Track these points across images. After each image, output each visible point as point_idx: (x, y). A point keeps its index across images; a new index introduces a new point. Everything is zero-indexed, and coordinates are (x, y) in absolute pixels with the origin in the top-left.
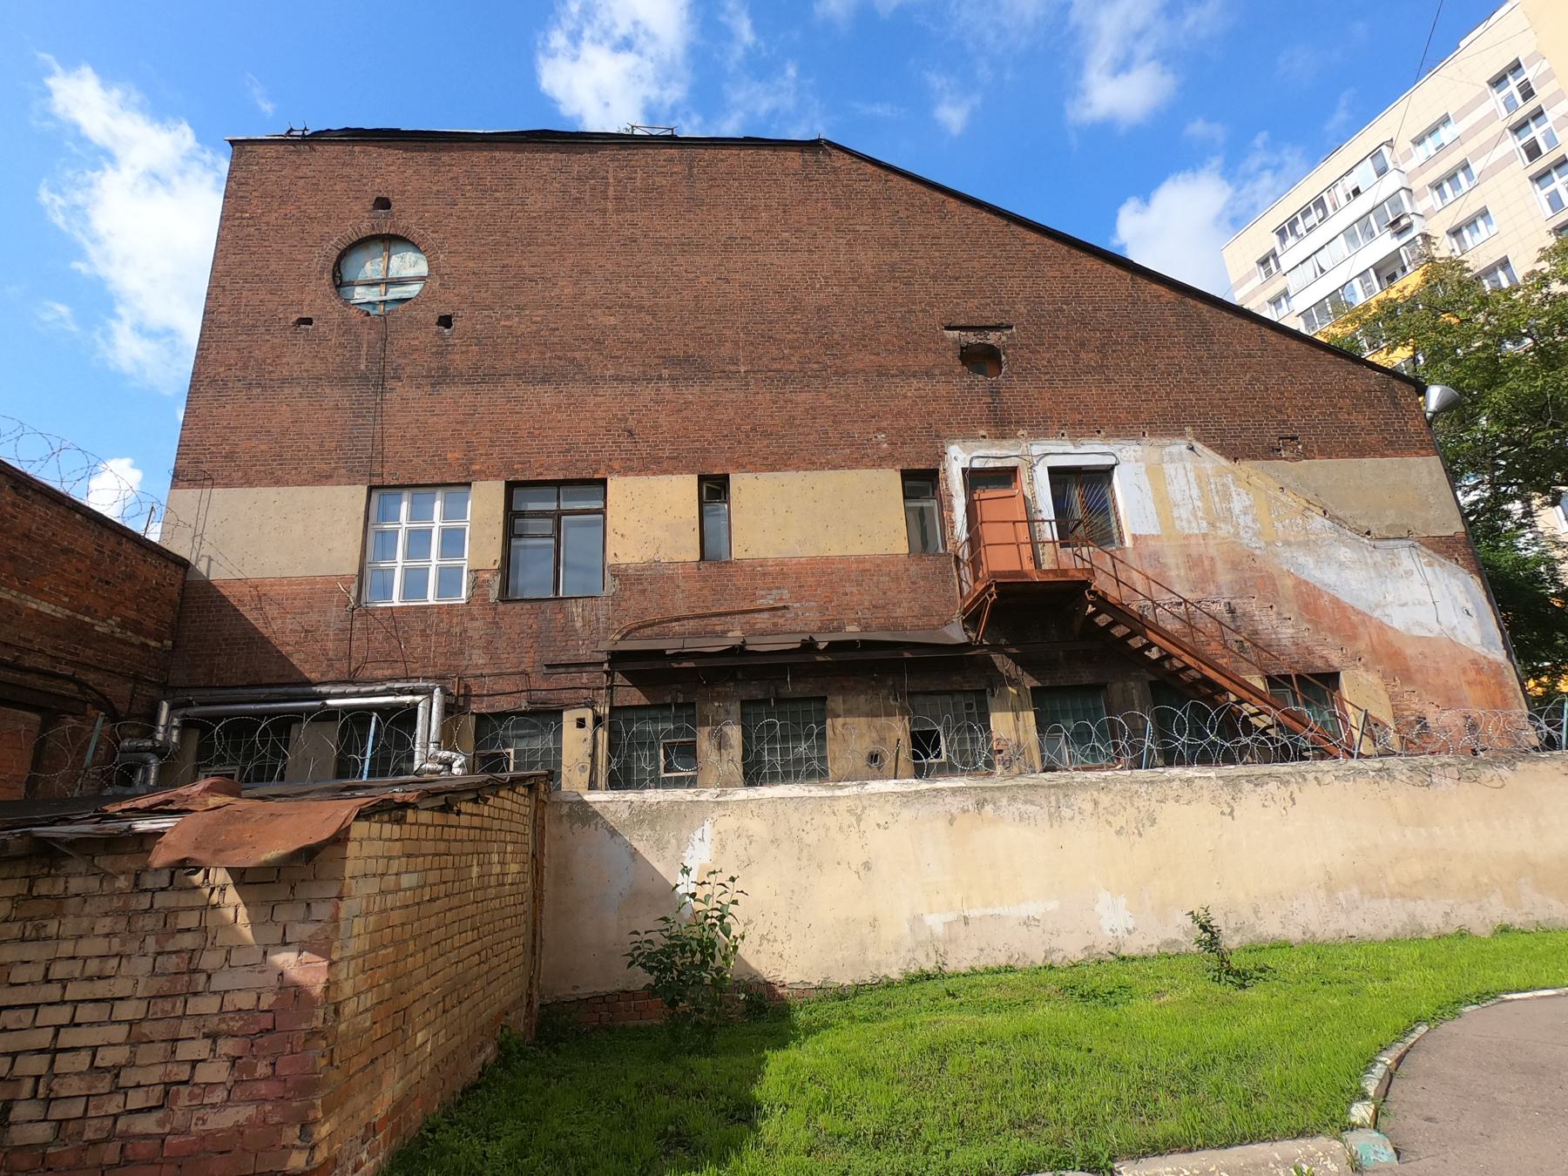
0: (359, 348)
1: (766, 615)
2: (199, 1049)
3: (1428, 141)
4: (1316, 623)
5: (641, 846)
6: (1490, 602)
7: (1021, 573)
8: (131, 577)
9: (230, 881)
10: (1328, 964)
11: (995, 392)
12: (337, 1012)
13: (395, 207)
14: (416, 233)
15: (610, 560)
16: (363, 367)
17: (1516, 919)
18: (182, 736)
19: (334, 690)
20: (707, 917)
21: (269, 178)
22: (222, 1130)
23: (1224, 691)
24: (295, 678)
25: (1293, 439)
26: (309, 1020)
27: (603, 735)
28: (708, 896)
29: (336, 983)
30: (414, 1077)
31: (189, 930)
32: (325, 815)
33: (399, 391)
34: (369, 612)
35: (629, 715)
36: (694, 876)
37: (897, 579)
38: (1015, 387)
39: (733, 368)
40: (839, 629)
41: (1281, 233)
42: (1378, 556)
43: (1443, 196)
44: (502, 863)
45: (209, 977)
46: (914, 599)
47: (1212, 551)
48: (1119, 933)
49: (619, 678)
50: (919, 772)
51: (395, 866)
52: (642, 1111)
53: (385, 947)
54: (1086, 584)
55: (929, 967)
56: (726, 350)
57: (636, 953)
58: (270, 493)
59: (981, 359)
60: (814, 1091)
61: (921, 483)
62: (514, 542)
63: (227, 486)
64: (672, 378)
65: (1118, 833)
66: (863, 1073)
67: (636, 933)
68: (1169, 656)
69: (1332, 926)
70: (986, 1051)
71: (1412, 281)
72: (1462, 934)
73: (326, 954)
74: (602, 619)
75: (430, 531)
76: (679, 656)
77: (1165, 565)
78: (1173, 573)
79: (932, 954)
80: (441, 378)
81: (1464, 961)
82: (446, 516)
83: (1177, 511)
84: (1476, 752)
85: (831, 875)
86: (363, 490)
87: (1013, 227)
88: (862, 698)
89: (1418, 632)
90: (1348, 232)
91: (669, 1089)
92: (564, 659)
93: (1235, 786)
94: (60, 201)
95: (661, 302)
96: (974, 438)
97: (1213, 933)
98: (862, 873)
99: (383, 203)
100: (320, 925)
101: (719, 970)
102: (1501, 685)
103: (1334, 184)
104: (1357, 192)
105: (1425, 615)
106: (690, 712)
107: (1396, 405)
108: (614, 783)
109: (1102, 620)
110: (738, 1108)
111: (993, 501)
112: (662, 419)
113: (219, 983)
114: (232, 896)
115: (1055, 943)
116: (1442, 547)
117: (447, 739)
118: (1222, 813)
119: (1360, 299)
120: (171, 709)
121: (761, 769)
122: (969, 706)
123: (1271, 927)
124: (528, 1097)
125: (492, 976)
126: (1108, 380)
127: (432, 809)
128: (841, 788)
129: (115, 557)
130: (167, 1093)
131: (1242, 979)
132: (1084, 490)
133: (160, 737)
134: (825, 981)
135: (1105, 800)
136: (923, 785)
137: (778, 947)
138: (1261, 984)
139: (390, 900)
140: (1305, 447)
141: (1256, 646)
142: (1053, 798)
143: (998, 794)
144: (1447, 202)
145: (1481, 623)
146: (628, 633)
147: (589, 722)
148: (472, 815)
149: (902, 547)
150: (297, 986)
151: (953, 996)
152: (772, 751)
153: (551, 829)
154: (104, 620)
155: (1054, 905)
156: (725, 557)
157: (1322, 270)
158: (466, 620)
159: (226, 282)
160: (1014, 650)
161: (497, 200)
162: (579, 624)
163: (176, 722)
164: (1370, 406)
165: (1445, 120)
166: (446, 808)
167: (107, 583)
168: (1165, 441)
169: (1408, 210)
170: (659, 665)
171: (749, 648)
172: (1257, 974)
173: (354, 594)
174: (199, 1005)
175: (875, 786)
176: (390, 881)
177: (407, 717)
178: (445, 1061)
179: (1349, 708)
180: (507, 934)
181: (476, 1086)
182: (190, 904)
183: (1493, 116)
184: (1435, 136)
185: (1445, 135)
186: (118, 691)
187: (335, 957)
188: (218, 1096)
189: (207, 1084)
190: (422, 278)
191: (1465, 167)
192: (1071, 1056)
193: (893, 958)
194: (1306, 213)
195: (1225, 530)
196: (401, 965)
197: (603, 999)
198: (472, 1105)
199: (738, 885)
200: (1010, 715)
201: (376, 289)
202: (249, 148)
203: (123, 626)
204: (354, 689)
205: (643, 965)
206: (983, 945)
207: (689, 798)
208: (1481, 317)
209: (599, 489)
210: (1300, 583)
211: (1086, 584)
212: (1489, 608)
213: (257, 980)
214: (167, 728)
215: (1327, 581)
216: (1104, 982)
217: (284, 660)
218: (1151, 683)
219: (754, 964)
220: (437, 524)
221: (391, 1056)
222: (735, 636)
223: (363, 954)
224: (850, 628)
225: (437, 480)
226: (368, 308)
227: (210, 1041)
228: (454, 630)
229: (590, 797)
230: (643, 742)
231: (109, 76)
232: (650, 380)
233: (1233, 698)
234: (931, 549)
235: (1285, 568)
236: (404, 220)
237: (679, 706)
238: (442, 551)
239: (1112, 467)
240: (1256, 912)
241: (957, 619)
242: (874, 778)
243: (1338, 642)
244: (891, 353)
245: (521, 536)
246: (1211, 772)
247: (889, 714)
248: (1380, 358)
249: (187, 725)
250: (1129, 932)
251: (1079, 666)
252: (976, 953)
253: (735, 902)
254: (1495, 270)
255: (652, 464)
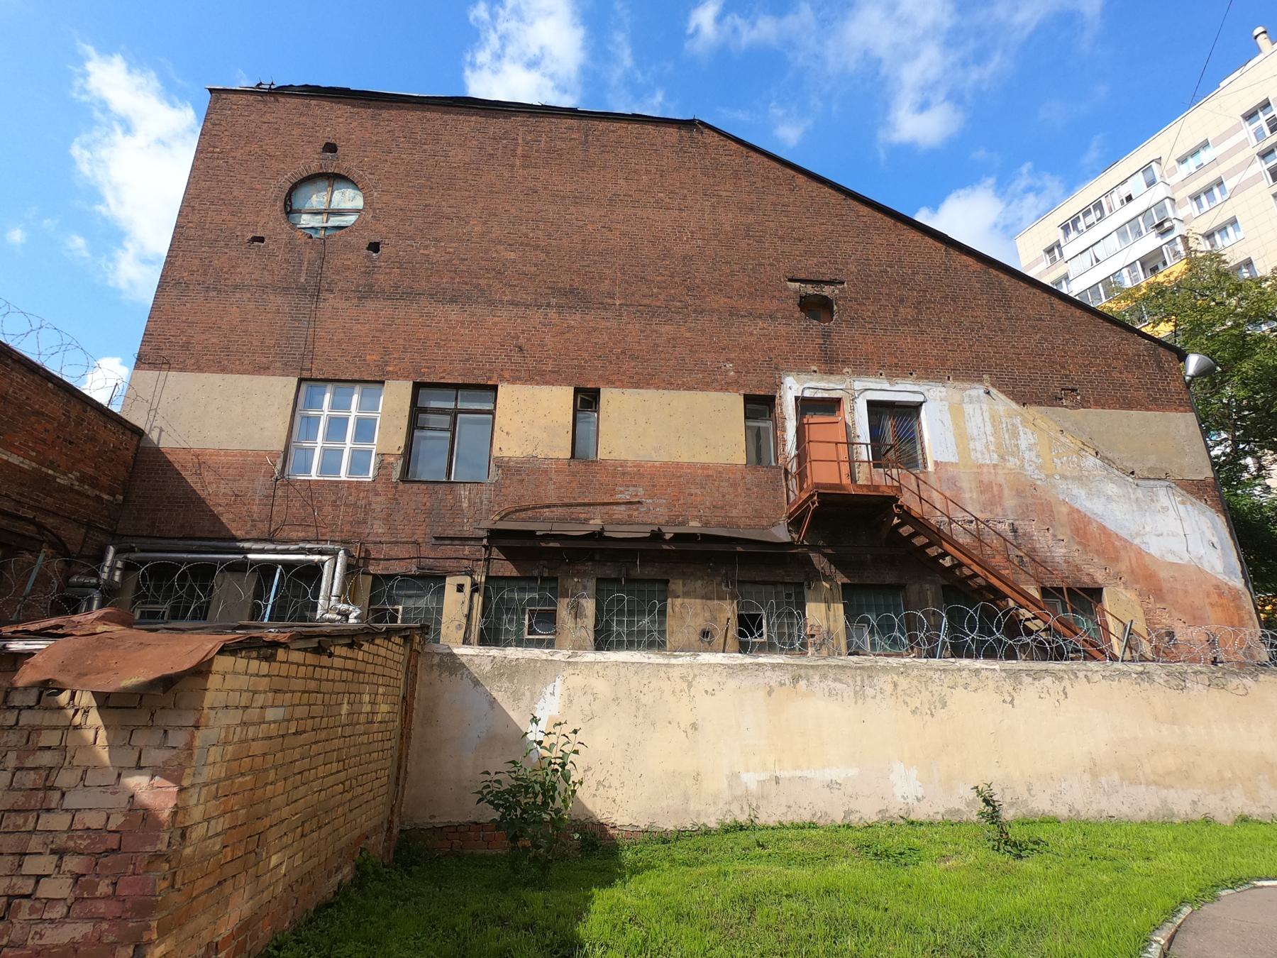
0: (301, 264)
1: (623, 508)
2: (44, 864)
3: (1190, 160)
4: (1085, 546)
5: (500, 697)
6: (1233, 538)
7: (839, 486)
8: (92, 439)
9: (94, 704)
10: (1095, 841)
11: (826, 335)
12: (183, 836)
13: (340, 151)
14: (355, 174)
15: (496, 453)
16: (302, 280)
17: (1255, 811)
18: (123, 577)
19: (255, 546)
20: (550, 763)
21: (232, 119)
22: (57, 946)
23: (1005, 597)
24: (223, 534)
25: (1073, 390)
26: (153, 843)
27: (478, 599)
28: (552, 745)
29: (184, 808)
30: (266, 896)
31: (49, 748)
32: (190, 648)
33: (331, 302)
34: (290, 483)
35: (502, 584)
36: (543, 725)
37: (734, 485)
38: (843, 332)
39: (609, 301)
40: (683, 524)
41: (1065, 228)
42: (1139, 493)
43: (1200, 206)
44: (373, 703)
45: (63, 795)
46: (748, 503)
47: (1001, 480)
48: (909, 801)
49: (495, 553)
50: (744, 648)
51: (260, 699)
52: (474, 941)
53: (242, 774)
54: (894, 499)
55: (743, 819)
56: (605, 286)
57: (485, 792)
58: (216, 378)
59: (817, 307)
60: (634, 932)
61: (760, 406)
62: (417, 433)
63: (181, 370)
64: (559, 306)
65: (914, 712)
66: (679, 918)
67: (488, 773)
68: (960, 565)
69: (1094, 806)
70: (794, 905)
71: (1175, 269)
72: (1208, 821)
73: (177, 780)
74: (485, 502)
75: (347, 419)
76: (548, 537)
77: (960, 488)
78: (967, 495)
79: (746, 808)
80: (367, 293)
81: (1215, 846)
82: (361, 407)
83: (974, 445)
84: (1218, 663)
85: (658, 732)
86: (294, 381)
87: (850, 201)
88: (699, 583)
89: (1171, 558)
90: (1121, 231)
91: (502, 921)
92: (451, 533)
93: (1016, 678)
94: (87, 154)
95: (554, 243)
96: (807, 372)
97: (994, 807)
98: (690, 732)
99: (331, 148)
100: (174, 752)
101: (558, 811)
102: (1238, 608)
103: (1111, 191)
104: (1129, 198)
105: (1177, 545)
106: (553, 585)
107: (1161, 368)
108: (483, 641)
109: (906, 530)
110: (563, 945)
111: (818, 424)
112: (548, 340)
113: (71, 801)
114: (94, 718)
115: (854, 805)
116: (1194, 489)
117: (349, 593)
118: (1004, 701)
119: (1128, 284)
120: (116, 553)
121: (609, 636)
122: (789, 596)
123: (1041, 804)
124: (373, 919)
125: (355, 803)
126: (922, 332)
127: (305, 650)
128: (676, 657)
129: (80, 421)
130: (9, 905)
131: (1018, 849)
132: (894, 422)
133: (105, 576)
134: (650, 826)
135: (903, 683)
136: (747, 659)
137: (612, 793)
138: (1036, 855)
139: (251, 732)
140: (1083, 398)
141: (1035, 560)
142: (859, 678)
143: (811, 672)
144: (1203, 210)
145: (1224, 555)
146: (506, 515)
147: (467, 589)
148: (345, 658)
149: (741, 459)
150: (146, 809)
151: (763, 846)
152: (620, 623)
153: (422, 676)
154: (65, 474)
155: (854, 772)
156: (592, 457)
157: (1097, 260)
158: (370, 495)
159: (196, 203)
160: (830, 551)
161: (425, 151)
162: (465, 505)
163: (119, 564)
164: (1139, 367)
165: (1205, 144)
166: (319, 650)
167: (71, 443)
168: (966, 385)
169: (1171, 215)
170: (529, 543)
171: (606, 534)
172: (1031, 846)
173: (279, 467)
174: (47, 822)
175: (706, 658)
176: (254, 714)
177: (314, 572)
178: (301, 881)
179: (1109, 619)
180: (373, 766)
181: (329, 905)
182: (54, 723)
183: (1244, 144)
184: (1196, 157)
185: (1205, 156)
186: (72, 535)
187: (185, 783)
188: (58, 912)
189: (48, 899)
190: (358, 211)
191: (1220, 183)
192: (868, 914)
193: (711, 809)
194: (1087, 213)
195: (1012, 462)
196: (259, 792)
197: (456, 828)
198: (321, 924)
199: (580, 737)
200: (823, 606)
201: (319, 217)
202: (224, 96)
203: (82, 480)
204: (271, 546)
205: (491, 803)
206: (792, 803)
207: (544, 657)
208: (1233, 301)
209: (490, 394)
210: (1074, 511)
211: (894, 499)
212: (1231, 542)
213: (109, 801)
214: (113, 568)
215: (1096, 511)
216: (895, 844)
217: (215, 518)
218: (943, 587)
219: (590, 806)
220: (353, 413)
221: (242, 878)
222: (595, 524)
223: (219, 781)
224: (692, 524)
225: (356, 377)
226: (311, 232)
227: (56, 857)
228: (359, 503)
229: (460, 650)
230: (508, 606)
231: (136, 62)
232: (539, 307)
233: (1011, 604)
234: (765, 462)
235: (1061, 497)
236: (346, 162)
237: (544, 579)
238: (353, 438)
239: (921, 404)
240: (1029, 790)
241: (783, 521)
242: (706, 651)
243: (1103, 562)
244: (742, 297)
245: (423, 428)
246: (996, 665)
247: (721, 598)
248: (1148, 330)
249: (129, 567)
250: (918, 800)
251: (882, 568)
252: (784, 809)
253: (576, 752)
254: (1240, 269)
255: (538, 376)
